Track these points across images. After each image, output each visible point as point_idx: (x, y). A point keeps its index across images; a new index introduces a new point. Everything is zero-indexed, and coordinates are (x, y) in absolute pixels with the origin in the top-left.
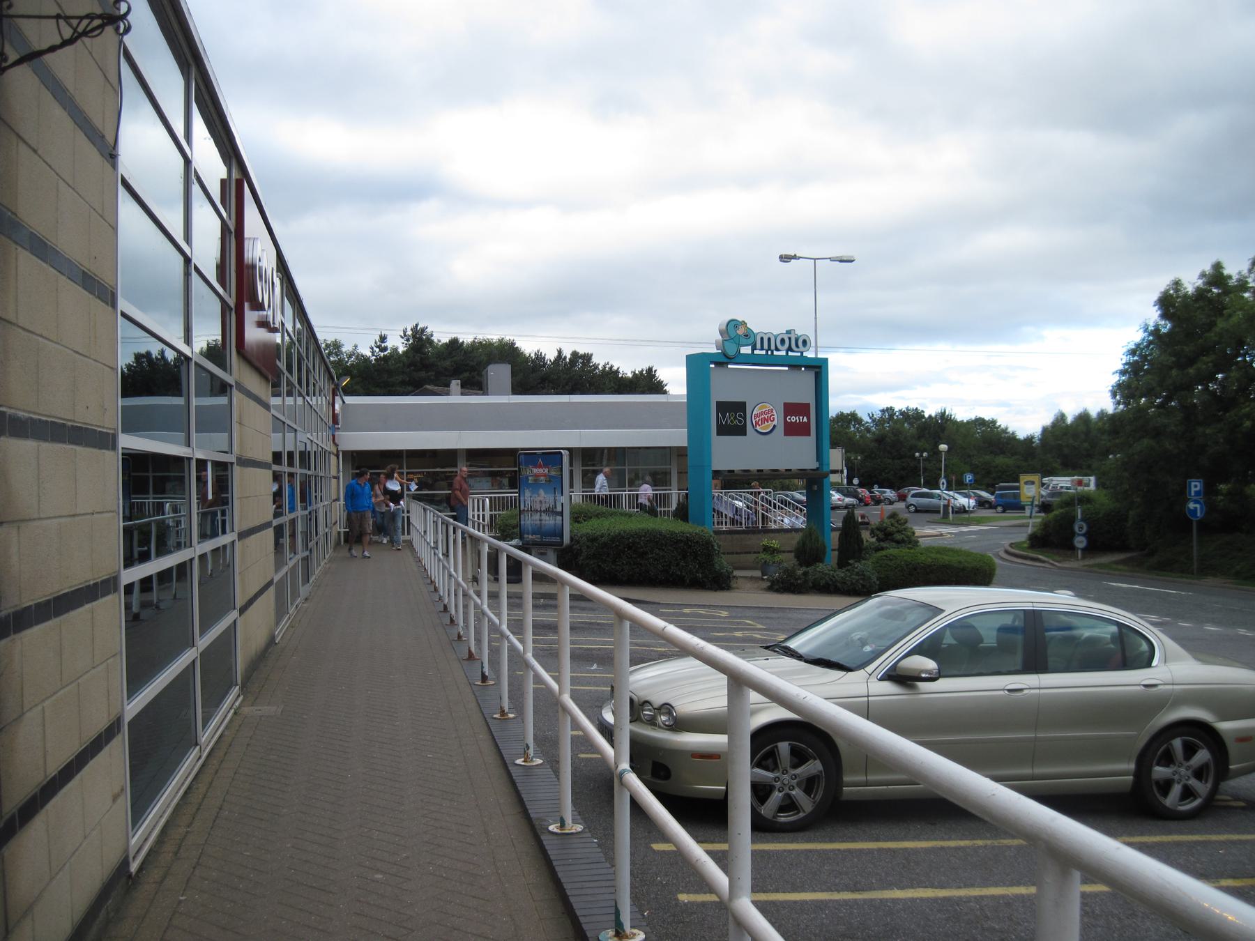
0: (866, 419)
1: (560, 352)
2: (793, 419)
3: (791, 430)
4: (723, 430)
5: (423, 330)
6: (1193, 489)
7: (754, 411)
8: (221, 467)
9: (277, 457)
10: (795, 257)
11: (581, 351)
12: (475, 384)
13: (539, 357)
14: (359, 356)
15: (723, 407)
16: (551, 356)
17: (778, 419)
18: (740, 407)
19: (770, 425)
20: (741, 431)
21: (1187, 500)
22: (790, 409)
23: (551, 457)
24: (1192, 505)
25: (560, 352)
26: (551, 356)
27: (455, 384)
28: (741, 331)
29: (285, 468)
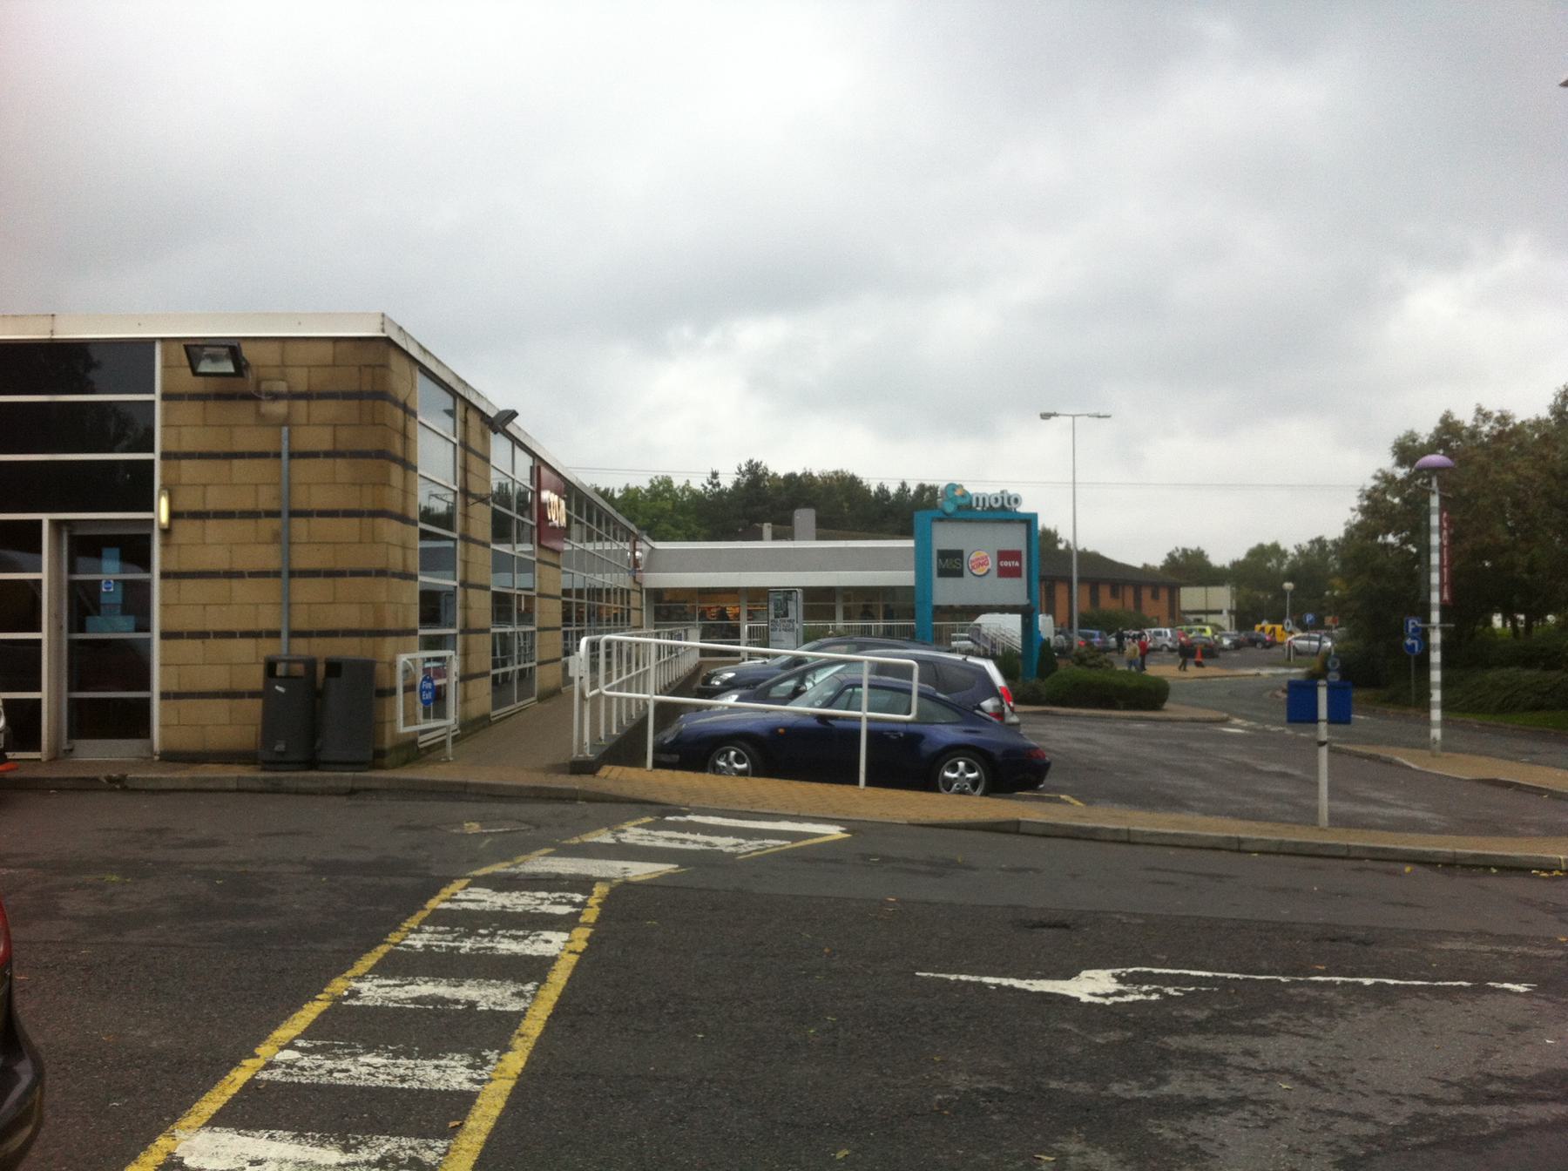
0: (1292, 550)
1: (904, 484)
2: (1006, 564)
3: (1004, 573)
4: (943, 573)
5: (757, 465)
6: (1411, 627)
7: (972, 557)
8: (529, 599)
9: (566, 592)
10: (1055, 415)
11: (928, 484)
12: (784, 530)
13: (882, 491)
14: (693, 492)
15: (943, 555)
16: (893, 489)
17: (992, 564)
18: (958, 555)
19: (985, 569)
20: (960, 574)
21: (1404, 638)
22: (1003, 555)
23: (757, 596)
24: (1409, 642)
25: (904, 484)
26: (893, 489)
27: (767, 528)
28: (958, 493)
29: (574, 600)
